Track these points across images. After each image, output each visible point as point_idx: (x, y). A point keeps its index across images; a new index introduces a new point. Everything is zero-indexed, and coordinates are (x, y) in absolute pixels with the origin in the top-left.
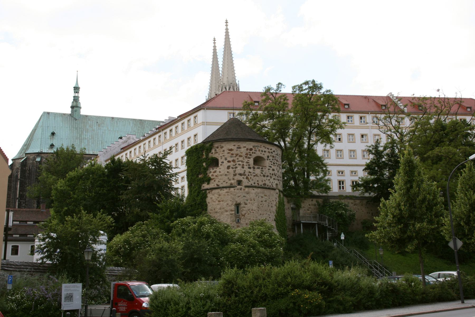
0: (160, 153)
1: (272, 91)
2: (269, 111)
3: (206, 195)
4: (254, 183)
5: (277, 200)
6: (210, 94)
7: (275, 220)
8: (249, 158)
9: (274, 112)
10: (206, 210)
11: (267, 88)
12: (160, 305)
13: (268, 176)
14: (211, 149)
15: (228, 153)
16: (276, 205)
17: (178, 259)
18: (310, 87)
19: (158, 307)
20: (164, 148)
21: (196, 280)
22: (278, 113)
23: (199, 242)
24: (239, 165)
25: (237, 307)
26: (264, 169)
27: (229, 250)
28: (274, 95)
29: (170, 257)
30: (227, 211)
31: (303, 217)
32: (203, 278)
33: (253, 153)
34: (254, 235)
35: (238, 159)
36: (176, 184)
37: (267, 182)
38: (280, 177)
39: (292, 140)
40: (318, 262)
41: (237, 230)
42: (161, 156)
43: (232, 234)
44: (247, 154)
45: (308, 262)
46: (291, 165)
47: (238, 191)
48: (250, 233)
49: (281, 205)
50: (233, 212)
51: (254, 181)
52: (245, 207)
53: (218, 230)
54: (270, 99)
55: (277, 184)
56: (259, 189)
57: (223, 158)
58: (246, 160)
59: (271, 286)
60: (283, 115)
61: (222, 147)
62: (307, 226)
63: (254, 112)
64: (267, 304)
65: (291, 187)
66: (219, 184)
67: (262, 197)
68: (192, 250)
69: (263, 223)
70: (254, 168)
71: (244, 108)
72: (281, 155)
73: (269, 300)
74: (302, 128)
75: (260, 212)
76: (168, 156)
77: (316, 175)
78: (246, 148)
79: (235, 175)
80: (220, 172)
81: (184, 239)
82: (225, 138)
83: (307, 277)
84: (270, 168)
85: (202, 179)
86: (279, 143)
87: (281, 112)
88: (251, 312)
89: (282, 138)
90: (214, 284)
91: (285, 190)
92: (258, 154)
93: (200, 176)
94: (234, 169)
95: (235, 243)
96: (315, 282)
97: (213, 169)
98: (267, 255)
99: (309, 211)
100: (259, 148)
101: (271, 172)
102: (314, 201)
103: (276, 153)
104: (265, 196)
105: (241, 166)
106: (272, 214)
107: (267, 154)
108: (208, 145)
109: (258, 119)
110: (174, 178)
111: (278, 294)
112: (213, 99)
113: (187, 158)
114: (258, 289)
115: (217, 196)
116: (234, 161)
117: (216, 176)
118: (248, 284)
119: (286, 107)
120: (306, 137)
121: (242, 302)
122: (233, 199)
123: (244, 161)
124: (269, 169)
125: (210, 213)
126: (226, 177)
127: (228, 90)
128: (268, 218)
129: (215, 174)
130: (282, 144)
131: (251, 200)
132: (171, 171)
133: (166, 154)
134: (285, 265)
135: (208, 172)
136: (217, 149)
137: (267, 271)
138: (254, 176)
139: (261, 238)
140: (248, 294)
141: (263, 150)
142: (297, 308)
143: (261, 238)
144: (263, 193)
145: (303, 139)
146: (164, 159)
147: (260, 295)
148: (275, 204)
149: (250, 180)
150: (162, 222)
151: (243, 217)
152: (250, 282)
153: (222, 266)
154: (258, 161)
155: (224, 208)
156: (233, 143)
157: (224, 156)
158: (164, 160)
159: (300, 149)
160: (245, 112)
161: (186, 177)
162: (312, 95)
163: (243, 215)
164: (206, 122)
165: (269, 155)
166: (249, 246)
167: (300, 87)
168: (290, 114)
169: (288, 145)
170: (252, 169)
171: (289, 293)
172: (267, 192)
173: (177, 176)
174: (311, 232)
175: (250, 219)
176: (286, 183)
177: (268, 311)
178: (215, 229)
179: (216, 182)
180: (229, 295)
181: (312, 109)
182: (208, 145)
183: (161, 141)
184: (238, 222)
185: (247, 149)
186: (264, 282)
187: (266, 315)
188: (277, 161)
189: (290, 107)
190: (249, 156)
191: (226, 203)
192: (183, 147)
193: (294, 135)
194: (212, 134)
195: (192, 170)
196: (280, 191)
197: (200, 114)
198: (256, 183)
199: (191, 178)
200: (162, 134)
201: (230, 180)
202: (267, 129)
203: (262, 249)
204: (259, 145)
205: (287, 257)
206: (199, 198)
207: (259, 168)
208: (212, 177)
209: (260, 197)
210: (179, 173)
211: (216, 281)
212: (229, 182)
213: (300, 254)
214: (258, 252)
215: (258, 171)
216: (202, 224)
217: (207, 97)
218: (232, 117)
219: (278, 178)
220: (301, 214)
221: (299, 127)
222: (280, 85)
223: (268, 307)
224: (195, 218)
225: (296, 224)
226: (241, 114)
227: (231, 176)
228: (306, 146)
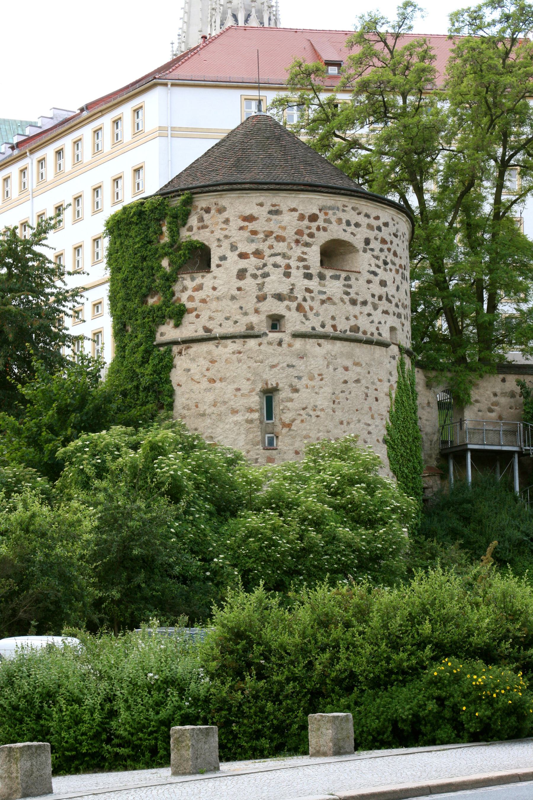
0: (25, 225)
1: (382, 30)
2: (374, 94)
3: (172, 359)
4: (323, 326)
5: (395, 378)
6: (184, 35)
7: (385, 441)
8: (307, 245)
9: (389, 97)
10: (171, 406)
11: (367, 18)
12: (22, 704)
13: (365, 303)
14: (187, 215)
15: (241, 228)
16: (390, 395)
17: (82, 557)
18: (507, 17)
19: (16, 708)
20: (38, 210)
21: (134, 625)
22: (400, 102)
23: (148, 506)
24: (276, 266)
25: (262, 710)
26: (352, 282)
27: (243, 532)
28: (390, 42)
29: (58, 550)
30: (235, 412)
31: (474, 431)
32: (155, 622)
33: (318, 229)
34: (319, 486)
35: (271, 247)
36: (75, 324)
37: (363, 323)
38: (405, 307)
39: (444, 188)
40: (518, 574)
41: (264, 471)
42: (28, 234)
43: (249, 483)
44: (299, 233)
45: (484, 571)
46: (438, 269)
47: (270, 350)
48: (305, 481)
49: (405, 395)
50: (256, 415)
51: (321, 319)
52: (291, 400)
53: (206, 472)
54: (376, 55)
55: (393, 329)
56: (338, 343)
57: (226, 244)
58: (298, 251)
59: (369, 648)
60: (417, 109)
61: (221, 210)
62: (484, 459)
63: (324, 97)
64: (356, 703)
65: (436, 338)
66: (210, 325)
67: (346, 369)
68: (125, 532)
69: (347, 449)
70: (322, 277)
71: (292, 85)
72: (407, 237)
73: (362, 691)
74: (478, 149)
75: (339, 415)
76: (51, 234)
77: (518, 302)
78: (296, 214)
79: (262, 298)
80: (214, 289)
81: (101, 496)
82: (232, 179)
83: (483, 620)
84: (371, 277)
85: (159, 309)
86: (403, 197)
87: (411, 98)
88: (304, 727)
89: (412, 180)
90: (192, 636)
91: (417, 348)
92: (336, 232)
93: (152, 301)
94: (260, 280)
95: (259, 510)
96: (505, 637)
97: (193, 279)
98: (359, 550)
99: (493, 415)
100: (340, 215)
101: (378, 290)
102: (511, 382)
103: (392, 229)
104: (357, 364)
105: (281, 270)
106: (378, 421)
107: (363, 233)
108: (177, 202)
109: (337, 120)
110: (70, 304)
111: (391, 672)
112: (193, 51)
113: (113, 243)
114: (327, 655)
115: (204, 363)
116: (258, 254)
117: (204, 301)
118: (297, 639)
119: (427, 80)
120: (488, 179)
121: (278, 695)
122: (256, 374)
123: (290, 253)
124: (369, 282)
125: (184, 417)
126: (235, 306)
127: (241, 23)
128: (364, 435)
129: (199, 295)
130: (413, 200)
131: (312, 378)
132: (59, 283)
133: (42, 230)
134: (415, 584)
135: (177, 288)
136: (206, 216)
137: (356, 600)
138: (323, 302)
139: (342, 495)
140: (298, 671)
141: (349, 219)
142: (447, 714)
143: (342, 495)
144: (350, 355)
145: (480, 186)
146: (37, 244)
147: (334, 674)
148: (386, 390)
149: (310, 315)
150: (34, 441)
151: (285, 430)
152: (303, 635)
153: (218, 579)
154: (333, 253)
155: (225, 403)
156: (256, 197)
157: (226, 237)
158: (37, 249)
159: (468, 216)
160: (295, 96)
161: (106, 303)
162: (513, 40)
163: (284, 425)
164: (173, 129)
165: (371, 234)
166: (303, 520)
167: (476, 17)
168: (439, 105)
169: (432, 203)
170: (316, 279)
171: (425, 668)
172: (361, 352)
173: (78, 299)
174: (499, 478)
175: (306, 437)
176: (421, 327)
177: (357, 723)
178: (199, 466)
179: (204, 321)
180: (239, 674)
181: (512, 86)
182: (177, 202)
183: (29, 186)
184: (270, 445)
185: (302, 217)
186: (348, 635)
187: (352, 736)
188: (395, 254)
189: (440, 82)
190: (306, 238)
191: (231, 388)
192: (97, 208)
193: (452, 171)
194: (191, 166)
195: (125, 280)
196: (401, 349)
197: (153, 100)
198: (329, 323)
199: (125, 307)
200: (30, 162)
201: (246, 314)
202: (364, 152)
203: (344, 531)
204: (340, 204)
205: (423, 556)
206: (149, 369)
207: (336, 277)
208: (189, 305)
209: (340, 370)
210: (85, 289)
211: (197, 629)
212: (244, 321)
213: (462, 547)
214: (333, 539)
215: (334, 288)
216: (157, 450)
217: (176, 46)
218: (253, 110)
219: (397, 311)
220: (468, 424)
221: (467, 147)
222: (409, 9)
223: (360, 712)
224: (137, 431)
225: (452, 454)
226: (282, 103)
227: (250, 303)
228: (487, 208)
